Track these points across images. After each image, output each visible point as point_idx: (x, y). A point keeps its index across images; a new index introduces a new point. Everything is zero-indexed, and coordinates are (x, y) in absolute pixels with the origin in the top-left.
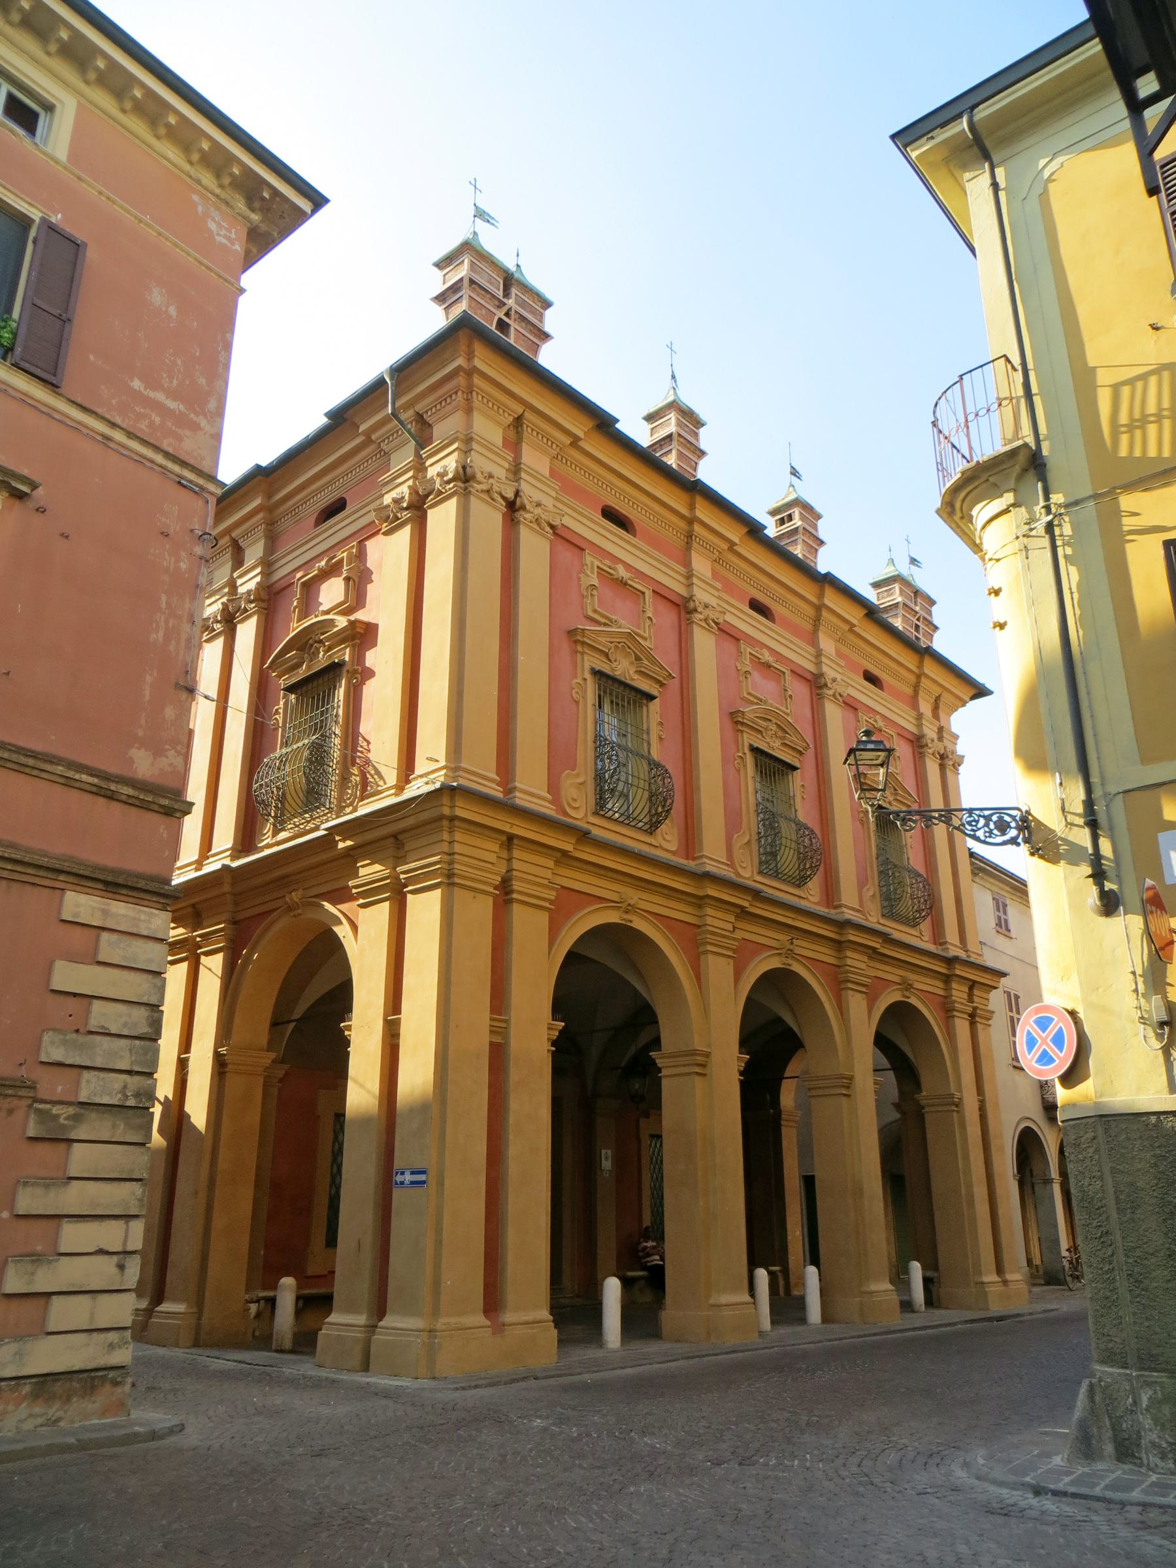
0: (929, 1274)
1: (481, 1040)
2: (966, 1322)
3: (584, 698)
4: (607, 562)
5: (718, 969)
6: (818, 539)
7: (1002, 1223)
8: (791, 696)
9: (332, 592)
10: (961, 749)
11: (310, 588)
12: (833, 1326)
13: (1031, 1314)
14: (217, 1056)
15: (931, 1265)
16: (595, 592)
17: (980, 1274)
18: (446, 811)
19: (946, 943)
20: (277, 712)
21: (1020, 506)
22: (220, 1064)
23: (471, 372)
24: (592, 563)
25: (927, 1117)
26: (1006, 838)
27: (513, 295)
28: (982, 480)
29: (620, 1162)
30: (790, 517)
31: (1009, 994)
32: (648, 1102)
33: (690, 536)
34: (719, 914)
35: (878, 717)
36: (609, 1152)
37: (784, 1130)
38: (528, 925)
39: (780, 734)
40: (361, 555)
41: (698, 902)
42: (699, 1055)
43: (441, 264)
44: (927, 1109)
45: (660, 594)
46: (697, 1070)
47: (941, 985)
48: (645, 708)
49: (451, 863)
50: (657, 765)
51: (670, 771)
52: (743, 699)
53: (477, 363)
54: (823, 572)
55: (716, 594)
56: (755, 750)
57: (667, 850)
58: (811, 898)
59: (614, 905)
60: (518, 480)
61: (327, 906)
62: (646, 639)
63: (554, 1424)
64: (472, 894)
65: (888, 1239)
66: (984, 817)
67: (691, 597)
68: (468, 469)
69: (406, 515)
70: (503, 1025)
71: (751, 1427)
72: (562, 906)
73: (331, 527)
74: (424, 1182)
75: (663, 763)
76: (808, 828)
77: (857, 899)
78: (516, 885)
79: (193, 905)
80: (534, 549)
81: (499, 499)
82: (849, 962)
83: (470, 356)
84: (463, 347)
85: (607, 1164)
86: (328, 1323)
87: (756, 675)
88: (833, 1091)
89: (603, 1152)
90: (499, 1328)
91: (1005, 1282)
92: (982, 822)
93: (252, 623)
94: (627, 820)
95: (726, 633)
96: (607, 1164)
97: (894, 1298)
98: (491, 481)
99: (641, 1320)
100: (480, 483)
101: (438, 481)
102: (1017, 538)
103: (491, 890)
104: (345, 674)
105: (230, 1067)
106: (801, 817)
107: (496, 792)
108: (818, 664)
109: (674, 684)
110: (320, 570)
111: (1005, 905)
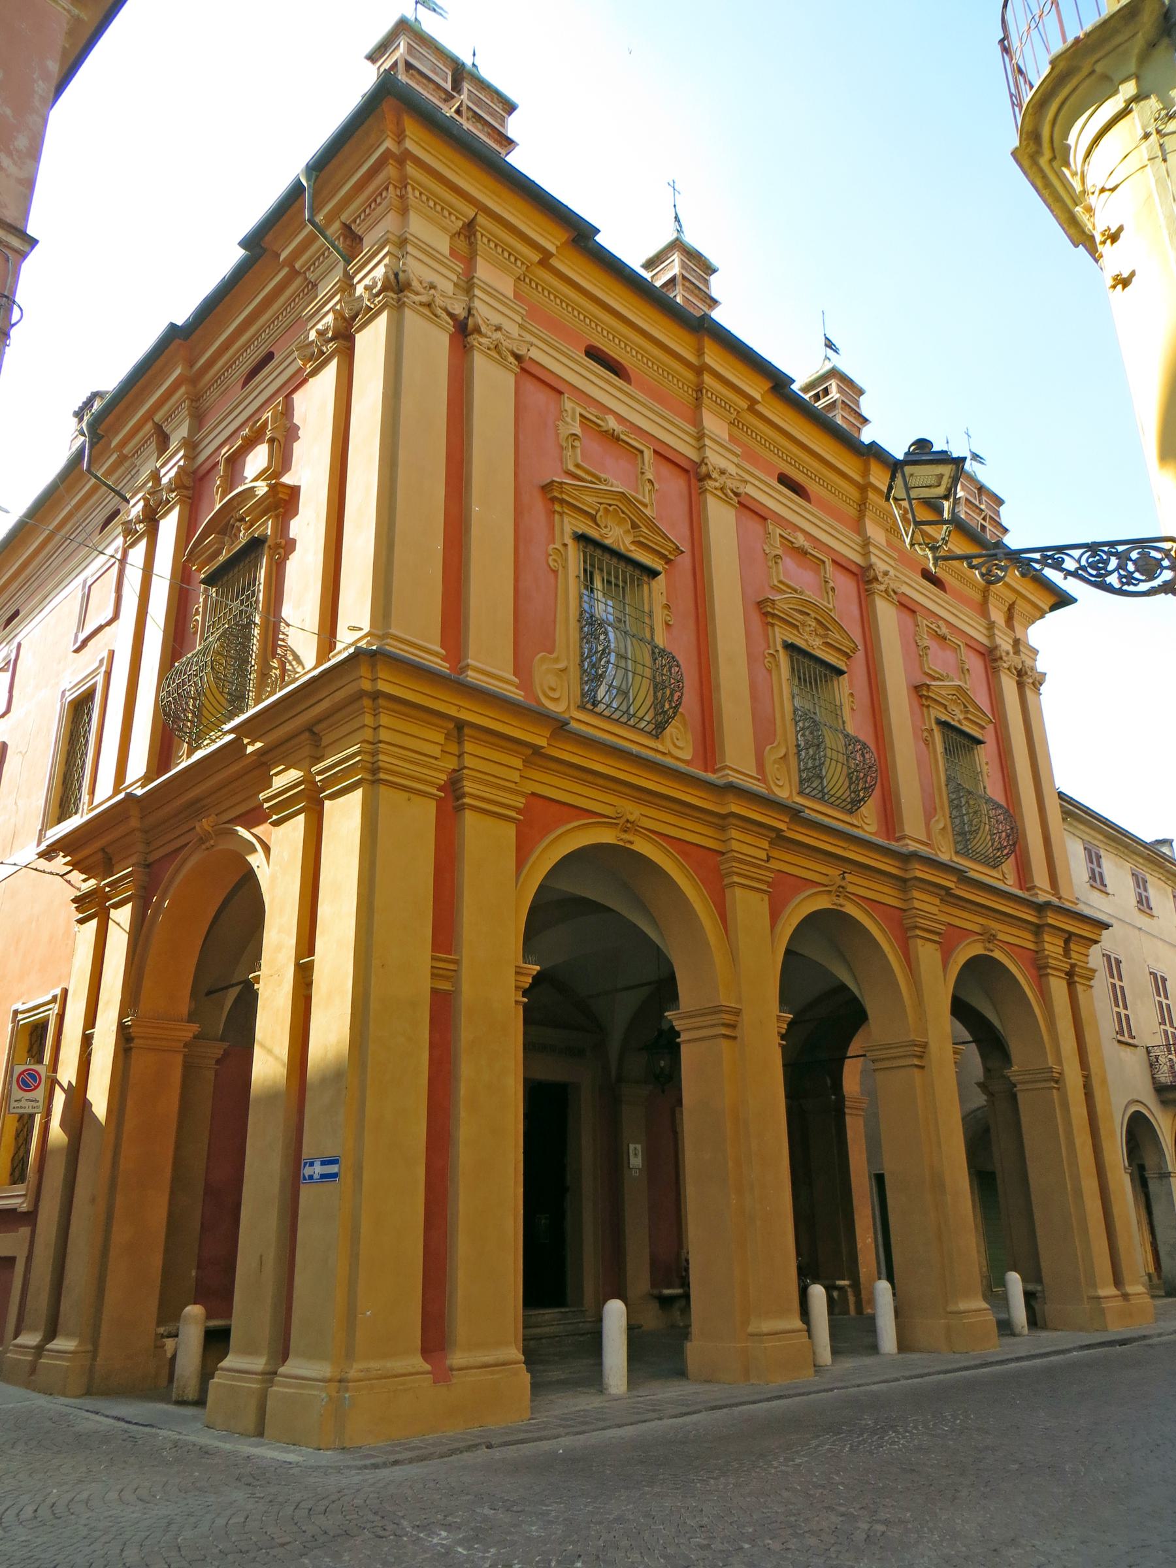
0: (1030, 1287)
1: (419, 985)
2: (1083, 1348)
3: (565, 567)
4: (593, 410)
5: (749, 906)
6: (860, 415)
7: (1118, 1225)
8: (833, 589)
9: (257, 460)
10: (1041, 666)
11: (235, 461)
12: (914, 1356)
13: (1160, 1335)
14: (122, 1028)
15: (1032, 1276)
16: (577, 443)
17: (1094, 1286)
18: (366, 685)
19: (1034, 887)
20: (197, 613)
21: (1147, 97)
22: (124, 1035)
23: (404, 158)
24: (574, 410)
25: (1020, 1096)
26: (1155, 583)
27: (465, 91)
28: (1085, 71)
29: (651, 1157)
30: (826, 392)
31: (1109, 957)
32: (667, 1080)
33: (699, 389)
34: (749, 839)
35: (941, 623)
36: (639, 1147)
37: (848, 1119)
38: (486, 841)
39: (821, 631)
40: (288, 410)
41: (720, 822)
42: (726, 1012)
43: (372, 57)
44: (1019, 1087)
45: (664, 456)
46: (724, 1031)
47: (1031, 937)
48: (646, 587)
49: (374, 754)
50: (663, 652)
51: (681, 662)
52: (774, 588)
53: (409, 144)
54: (867, 443)
55: (736, 460)
56: (790, 647)
57: (678, 759)
58: (865, 826)
59: (610, 822)
60: (472, 297)
61: (242, 831)
62: (646, 506)
63: (460, 1543)
64: (406, 795)
65: (978, 1246)
66: (1117, 554)
67: (703, 461)
68: (401, 275)
69: (332, 346)
70: (452, 967)
71: (775, 1545)
72: (535, 819)
73: (257, 386)
74: (335, 1175)
75: (668, 650)
76: (859, 741)
77: (922, 828)
78: (469, 787)
79: (103, 850)
80: (493, 384)
81: (444, 315)
82: (917, 904)
83: (400, 137)
84: (390, 125)
85: (636, 1161)
86: (223, 1369)
87: (789, 563)
88: (902, 1062)
89: (632, 1146)
90: (442, 1375)
91: (1125, 1296)
92: (1113, 563)
93: (174, 516)
94: (627, 720)
95: (747, 507)
96: (636, 1161)
97: (991, 1318)
98: (432, 291)
99: (658, 1352)
100: (417, 294)
101: (366, 296)
102: (1147, 136)
103: (435, 791)
104: (266, 550)
105: (136, 1041)
106: (850, 729)
107: (443, 667)
108: (866, 554)
109: (685, 561)
110: (245, 438)
111: (1099, 857)
